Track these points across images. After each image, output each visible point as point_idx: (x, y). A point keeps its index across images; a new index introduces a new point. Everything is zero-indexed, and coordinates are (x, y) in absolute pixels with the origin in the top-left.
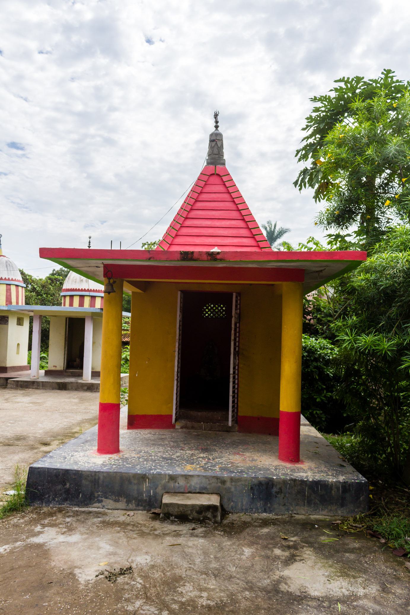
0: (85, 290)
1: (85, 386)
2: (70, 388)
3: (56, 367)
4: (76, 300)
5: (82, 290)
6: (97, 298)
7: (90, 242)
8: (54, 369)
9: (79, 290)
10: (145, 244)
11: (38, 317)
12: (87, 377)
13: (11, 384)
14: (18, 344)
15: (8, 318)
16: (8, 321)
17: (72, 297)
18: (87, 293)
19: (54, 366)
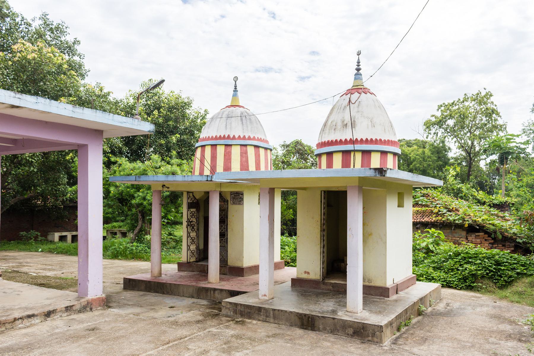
1: (350, 327)
2: (321, 327)
3: (308, 273)
4: (338, 159)
6: (373, 154)
7: (359, 62)
8: (305, 276)
9: (341, 142)
10: (441, 106)
11: (267, 191)
13: (226, 308)
15: (242, 194)
16: (242, 200)
18: (358, 147)
19: (305, 272)
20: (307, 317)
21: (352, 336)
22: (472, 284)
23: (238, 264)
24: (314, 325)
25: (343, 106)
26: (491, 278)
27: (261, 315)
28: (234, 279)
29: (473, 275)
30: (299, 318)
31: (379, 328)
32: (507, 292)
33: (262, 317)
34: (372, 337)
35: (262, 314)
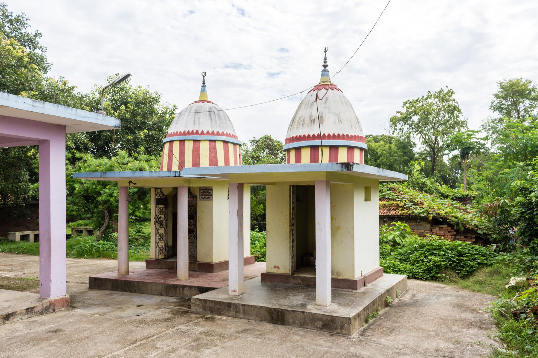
1: (319, 320)
2: (291, 321)
3: (278, 268)
4: (306, 154)
7: (325, 59)
8: (275, 271)
9: (309, 138)
10: (406, 103)
12: (324, 300)
15: (212, 190)
16: (212, 195)
17: (171, 142)
18: (325, 142)
19: (275, 267)
20: (277, 311)
22: (436, 275)
23: (207, 260)
24: (283, 319)
27: (231, 311)
30: (269, 313)
32: (469, 282)
33: (232, 312)
35: (231, 309)
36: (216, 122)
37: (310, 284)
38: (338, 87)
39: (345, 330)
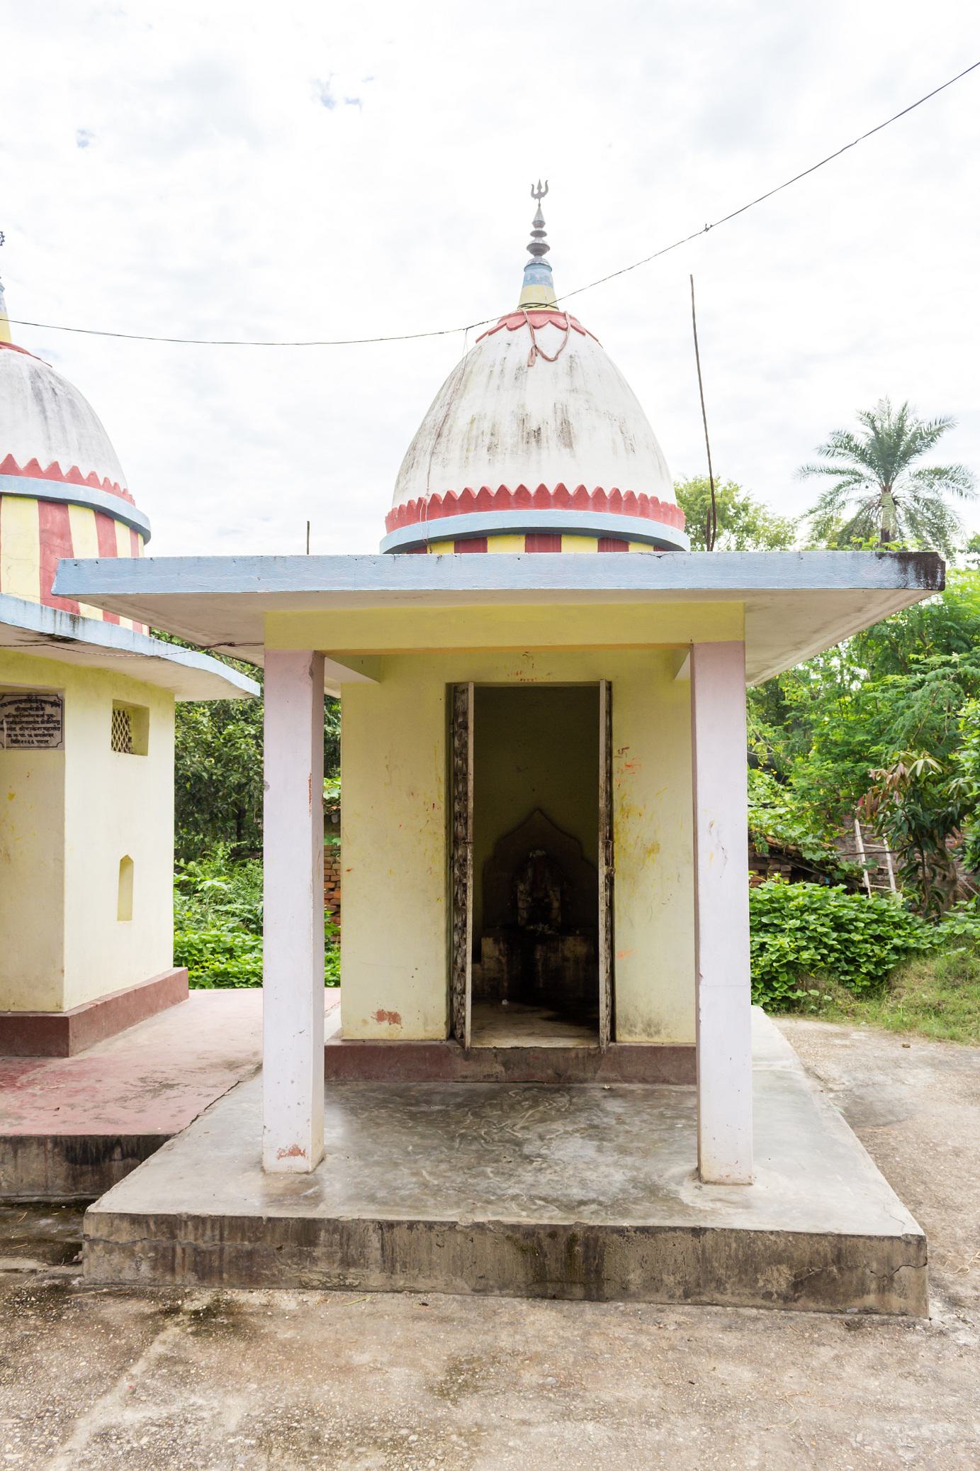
0: (561, 497)
1: (777, 1259)
2: (635, 1277)
3: (394, 1018)
5: (542, 498)
7: (539, 223)
8: (380, 1032)
9: (522, 497)
11: (306, 662)
13: (110, 1247)
14: (126, 863)
15: (59, 704)
16: (59, 726)
19: (381, 1016)
20: (563, 1239)
21: (787, 1300)
22: (790, 994)
23: (37, 1003)
24: (598, 1272)
25: (511, 366)
26: (832, 969)
27: (314, 1261)
28: (36, 1074)
29: (791, 966)
30: (523, 1250)
31: (912, 1250)
32: (885, 1008)
33: (323, 1266)
34: (882, 1290)
35: (318, 1252)
36: (63, 429)
37: (539, 1075)
38: (585, 325)
39: (903, 1294)
